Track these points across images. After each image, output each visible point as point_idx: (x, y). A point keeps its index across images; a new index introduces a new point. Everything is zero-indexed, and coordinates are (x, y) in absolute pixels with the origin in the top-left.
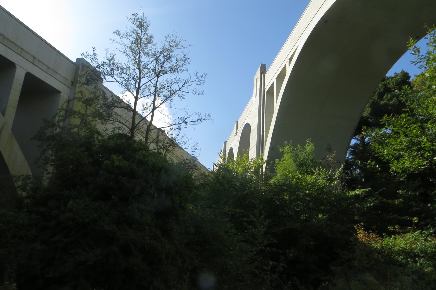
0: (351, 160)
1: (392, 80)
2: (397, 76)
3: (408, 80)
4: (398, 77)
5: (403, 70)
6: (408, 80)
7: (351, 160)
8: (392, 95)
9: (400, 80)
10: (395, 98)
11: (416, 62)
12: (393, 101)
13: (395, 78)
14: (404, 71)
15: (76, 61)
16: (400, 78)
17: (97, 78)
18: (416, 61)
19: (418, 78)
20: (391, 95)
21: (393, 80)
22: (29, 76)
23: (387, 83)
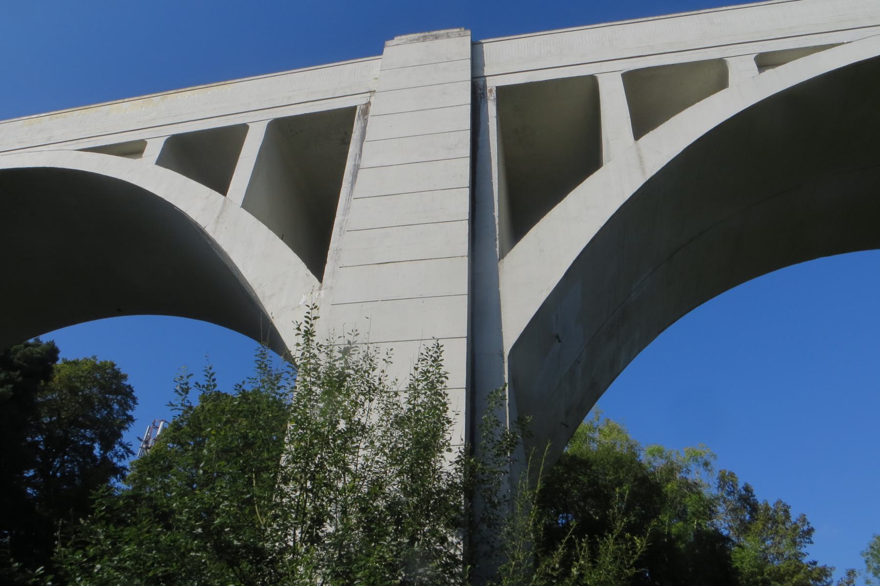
0: (576, 507)
1: (24, 349)
2: (38, 346)
3: (50, 363)
4: (38, 350)
5: (53, 341)
6: (50, 363)
7: (576, 507)
8: (8, 377)
9: (38, 355)
10: (10, 386)
11: (176, 407)
12: (4, 389)
13: (32, 348)
14: (54, 344)
15: (469, 32)
16: (39, 353)
17: (514, 423)
18: (177, 406)
19: (68, 367)
20: (5, 376)
21: (26, 349)
22: (221, 185)
23: (12, 350)
